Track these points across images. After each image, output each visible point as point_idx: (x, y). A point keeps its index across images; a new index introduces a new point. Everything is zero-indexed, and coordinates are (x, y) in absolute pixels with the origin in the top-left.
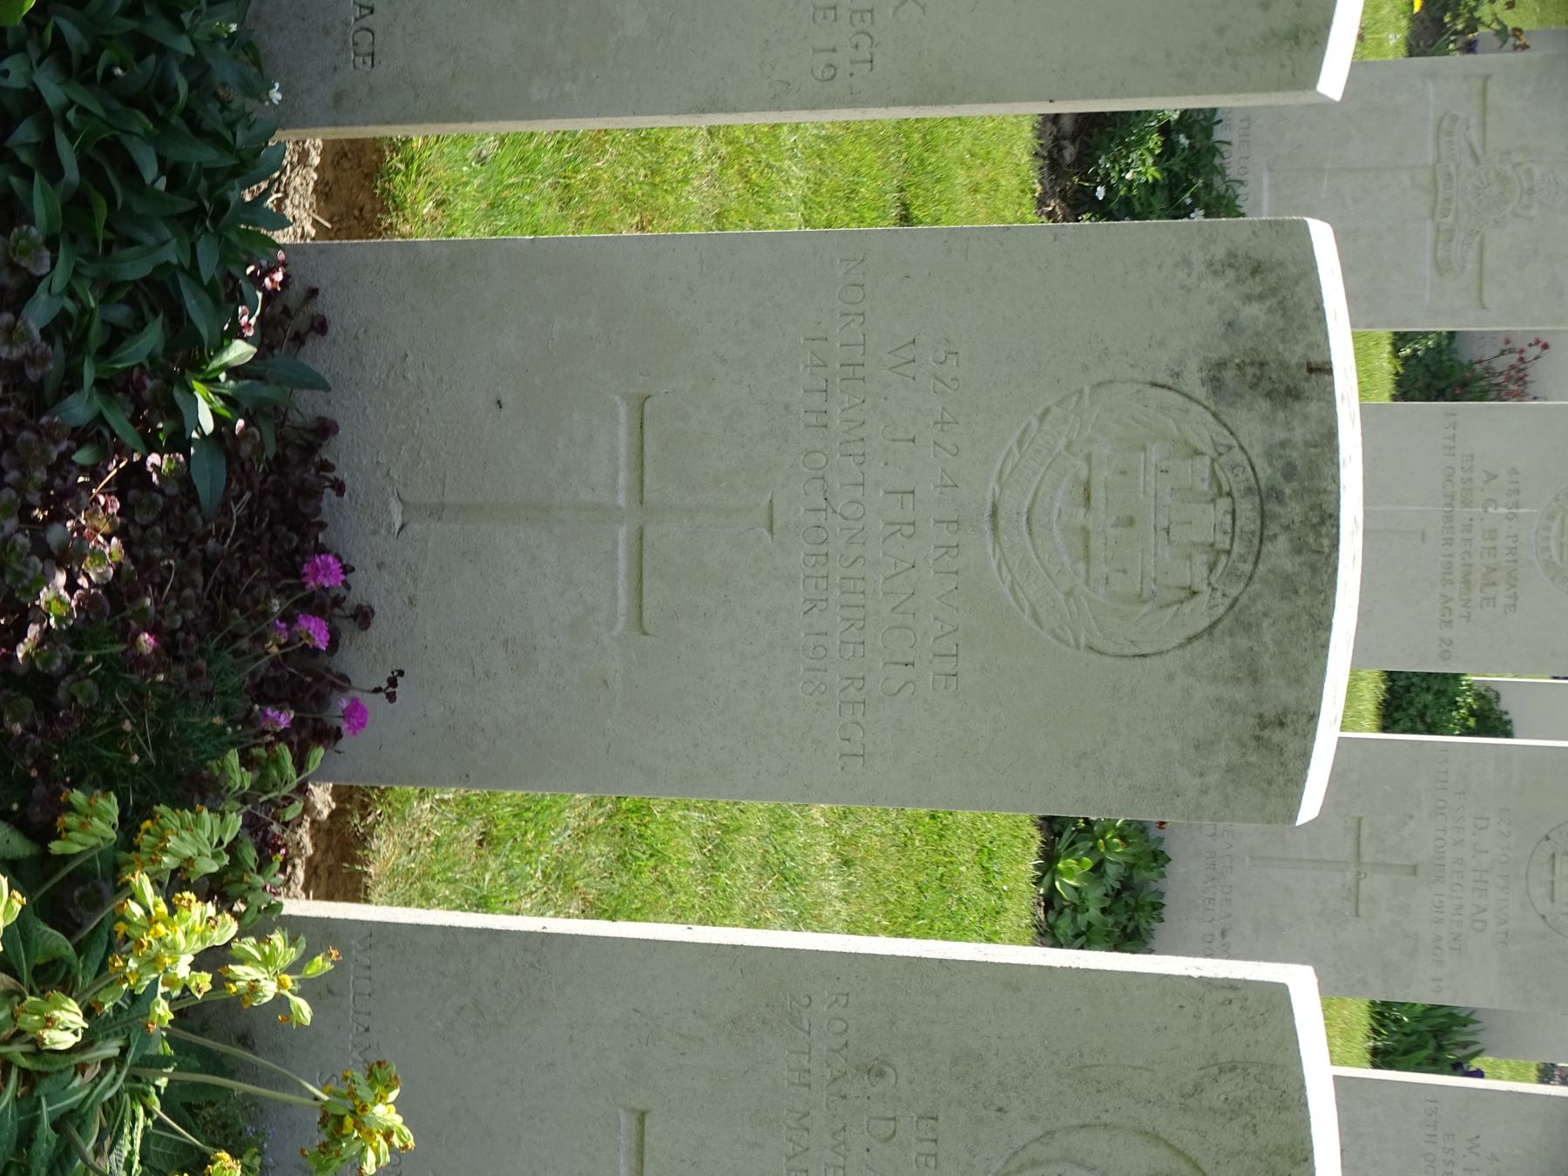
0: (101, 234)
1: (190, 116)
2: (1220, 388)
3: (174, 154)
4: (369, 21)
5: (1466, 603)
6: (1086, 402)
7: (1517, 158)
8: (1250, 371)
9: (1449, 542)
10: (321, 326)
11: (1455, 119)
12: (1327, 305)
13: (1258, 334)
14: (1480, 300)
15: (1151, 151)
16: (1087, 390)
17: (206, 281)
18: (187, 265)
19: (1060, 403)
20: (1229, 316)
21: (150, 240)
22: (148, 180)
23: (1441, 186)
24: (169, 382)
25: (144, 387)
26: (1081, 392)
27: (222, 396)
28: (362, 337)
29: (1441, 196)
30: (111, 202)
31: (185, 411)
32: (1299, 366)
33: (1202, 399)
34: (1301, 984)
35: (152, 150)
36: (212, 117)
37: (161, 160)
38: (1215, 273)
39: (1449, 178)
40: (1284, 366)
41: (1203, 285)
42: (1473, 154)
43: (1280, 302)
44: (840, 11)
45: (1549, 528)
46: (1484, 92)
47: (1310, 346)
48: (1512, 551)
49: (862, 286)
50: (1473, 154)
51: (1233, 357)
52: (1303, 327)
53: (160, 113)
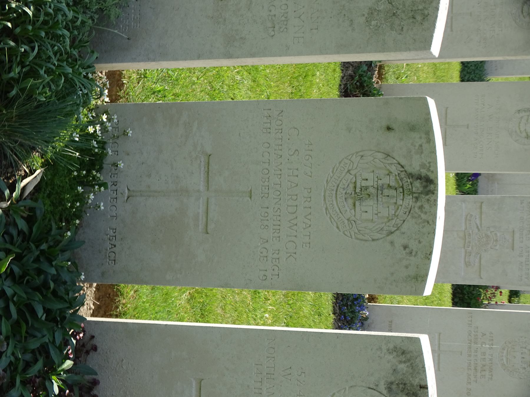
0: (24, 334)
1: (55, 293)
2: (391, 391)
3: (48, 306)
4: (114, 249)
5: (476, 377)
6: (347, 392)
7: (492, 230)
8: (401, 386)
9: (470, 356)
10: (95, 348)
11: (471, 216)
12: (426, 366)
13: (403, 374)
14: (480, 275)
16: (347, 388)
17: (58, 345)
18: (51, 340)
19: (338, 392)
20: (394, 368)
21: (39, 335)
22: (39, 317)
23: (467, 237)
24: (44, 379)
25: (36, 382)
26: (345, 389)
27: (62, 380)
28: (108, 353)
29: (467, 241)
30: (27, 322)
31: (49, 390)
32: (417, 386)
33: (385, 394)
35: (41, 306)
36: (61, 291)
37: (44, 308)
38: (390, 353)
40: (412, 385)
41: (386, 356)
42: (477, 227)
43: (411, 364)
44: (268, 258)
45: (503, 353)
46: (481, 207)
47: (421, 379)
48: (491, 360)
49: (274, 348)
50: (477, 227)
51: (395, 381)
52: (418, 373)
53: (44, 294)
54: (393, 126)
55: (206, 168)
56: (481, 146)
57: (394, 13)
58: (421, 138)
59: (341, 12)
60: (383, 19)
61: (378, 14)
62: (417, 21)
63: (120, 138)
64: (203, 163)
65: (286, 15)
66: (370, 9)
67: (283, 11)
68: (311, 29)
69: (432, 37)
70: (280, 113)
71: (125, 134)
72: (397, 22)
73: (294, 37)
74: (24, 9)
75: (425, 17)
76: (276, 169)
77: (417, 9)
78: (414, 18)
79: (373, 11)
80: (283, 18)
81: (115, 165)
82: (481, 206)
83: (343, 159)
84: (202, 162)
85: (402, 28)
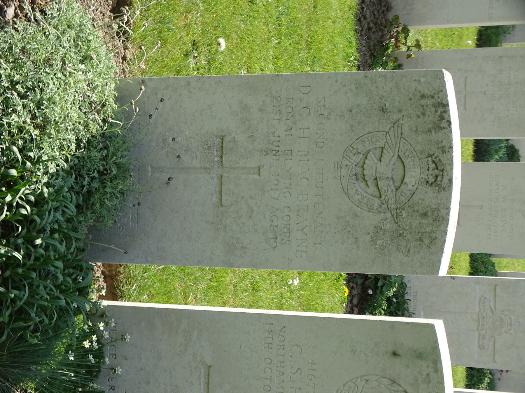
7: (506, 313)
11: (485, 298)
15: (383, 310)
29: (481, 324)
34: (439, 325)
39: (483, 317)
42: (491, 310)
46: (495, 290)
50: (491, 310)
54: (399, 351)
55: (206, 379)
56: (495, 228)
57: (400, 234)
58: (428, 367)
59: (345, 229)
60: (389, 239)
61: (384, 233)
62: (425, 244)
63: (118, 341)
64: (203, 374)
65: (288, 227)
66: (375, 227)
67: (285, 223)
68: (315, 244)
69: (440, 261)
70: (282, 329)
71: (123, 338)
72: (403, 243)
73: (297, 251)
74: (14, 254)
75: (433, 240)
76: (278, 386)
77: (424, 231)
78: (421, 240)
79: (379, 230)
80: (285, 230)
81: (113, 369)
82: (495, 288)
83: (347, 382)
84: (202, 372)
85: (409, 250)
